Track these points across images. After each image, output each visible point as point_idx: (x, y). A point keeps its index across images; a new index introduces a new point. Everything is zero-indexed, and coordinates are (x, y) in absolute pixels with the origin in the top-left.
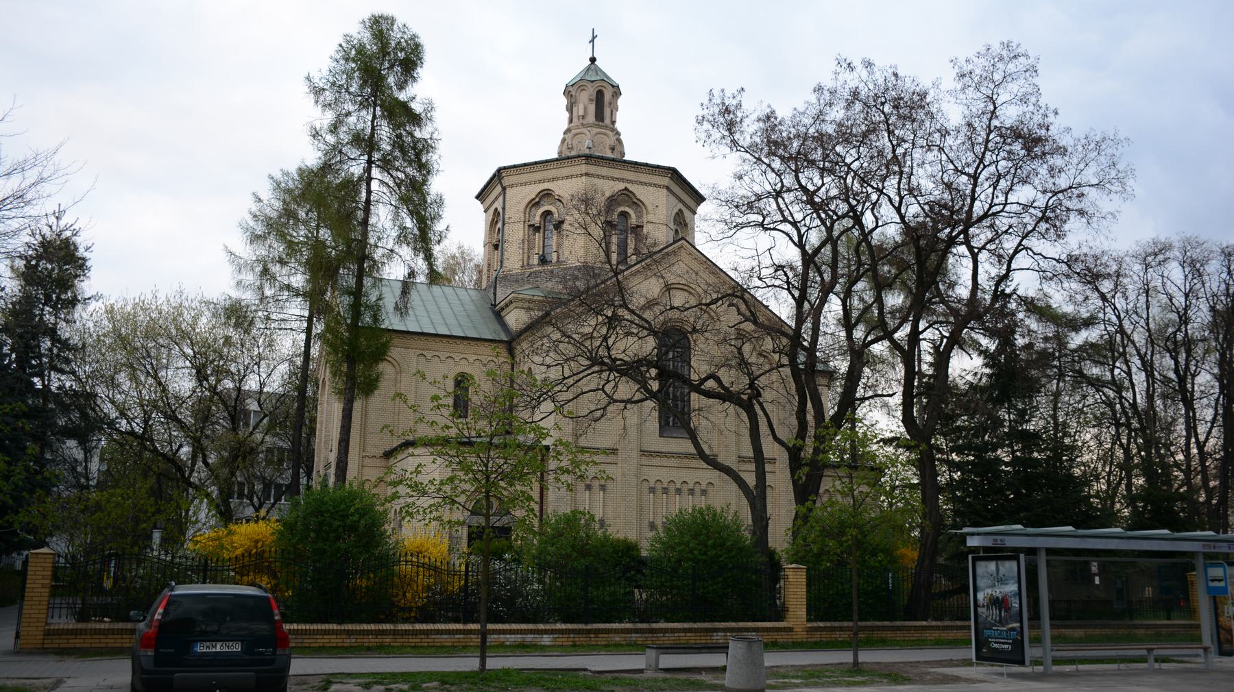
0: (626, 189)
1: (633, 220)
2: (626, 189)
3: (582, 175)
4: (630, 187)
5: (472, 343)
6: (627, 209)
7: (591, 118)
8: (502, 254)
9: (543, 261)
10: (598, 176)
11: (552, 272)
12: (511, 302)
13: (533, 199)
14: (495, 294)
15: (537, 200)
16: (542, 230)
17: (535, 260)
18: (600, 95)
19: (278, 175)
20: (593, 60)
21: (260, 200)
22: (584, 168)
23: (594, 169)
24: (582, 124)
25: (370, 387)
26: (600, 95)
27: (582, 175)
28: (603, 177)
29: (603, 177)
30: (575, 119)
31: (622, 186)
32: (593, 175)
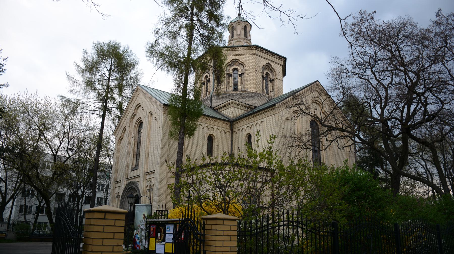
0: (269, 63)
1: (271, 77)
2: (269, 63)
3: (253, 54)
4: (271, 63)
5: (216, 120)
6: (269, 72)
7: (243, 36)
8: (207, 87)
9: (235, 89)
10: (259, 56)
11: (241, 94)
12: (229, 104)
13: (229, 63)
14: (211, 102)
15: (230, 63)
16: (205, 85)
17: (231, 88)
18: (245, 27)
19: (96, 42)
20: (239, 15)
21: (86, 53)
22: (254, 51)
23: (258, 53)
24: (240, 38)
25: (191, 133)
26: (245, 27)
27: (253, 54)
28: (261, 57)
29: (261, 57)
30: (235, 37)
31: (267, 62)
32: (258, 55)
